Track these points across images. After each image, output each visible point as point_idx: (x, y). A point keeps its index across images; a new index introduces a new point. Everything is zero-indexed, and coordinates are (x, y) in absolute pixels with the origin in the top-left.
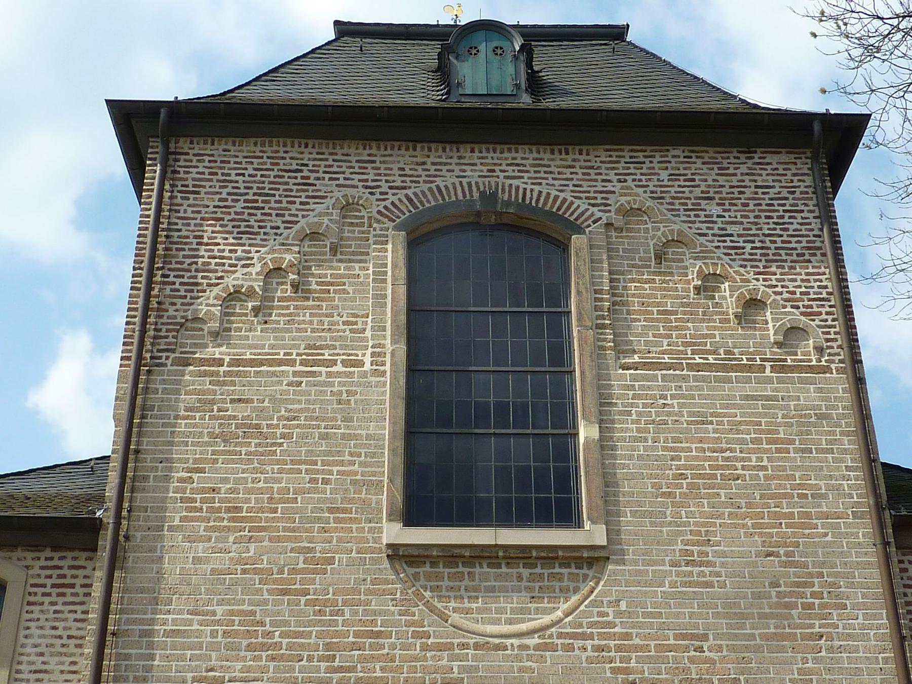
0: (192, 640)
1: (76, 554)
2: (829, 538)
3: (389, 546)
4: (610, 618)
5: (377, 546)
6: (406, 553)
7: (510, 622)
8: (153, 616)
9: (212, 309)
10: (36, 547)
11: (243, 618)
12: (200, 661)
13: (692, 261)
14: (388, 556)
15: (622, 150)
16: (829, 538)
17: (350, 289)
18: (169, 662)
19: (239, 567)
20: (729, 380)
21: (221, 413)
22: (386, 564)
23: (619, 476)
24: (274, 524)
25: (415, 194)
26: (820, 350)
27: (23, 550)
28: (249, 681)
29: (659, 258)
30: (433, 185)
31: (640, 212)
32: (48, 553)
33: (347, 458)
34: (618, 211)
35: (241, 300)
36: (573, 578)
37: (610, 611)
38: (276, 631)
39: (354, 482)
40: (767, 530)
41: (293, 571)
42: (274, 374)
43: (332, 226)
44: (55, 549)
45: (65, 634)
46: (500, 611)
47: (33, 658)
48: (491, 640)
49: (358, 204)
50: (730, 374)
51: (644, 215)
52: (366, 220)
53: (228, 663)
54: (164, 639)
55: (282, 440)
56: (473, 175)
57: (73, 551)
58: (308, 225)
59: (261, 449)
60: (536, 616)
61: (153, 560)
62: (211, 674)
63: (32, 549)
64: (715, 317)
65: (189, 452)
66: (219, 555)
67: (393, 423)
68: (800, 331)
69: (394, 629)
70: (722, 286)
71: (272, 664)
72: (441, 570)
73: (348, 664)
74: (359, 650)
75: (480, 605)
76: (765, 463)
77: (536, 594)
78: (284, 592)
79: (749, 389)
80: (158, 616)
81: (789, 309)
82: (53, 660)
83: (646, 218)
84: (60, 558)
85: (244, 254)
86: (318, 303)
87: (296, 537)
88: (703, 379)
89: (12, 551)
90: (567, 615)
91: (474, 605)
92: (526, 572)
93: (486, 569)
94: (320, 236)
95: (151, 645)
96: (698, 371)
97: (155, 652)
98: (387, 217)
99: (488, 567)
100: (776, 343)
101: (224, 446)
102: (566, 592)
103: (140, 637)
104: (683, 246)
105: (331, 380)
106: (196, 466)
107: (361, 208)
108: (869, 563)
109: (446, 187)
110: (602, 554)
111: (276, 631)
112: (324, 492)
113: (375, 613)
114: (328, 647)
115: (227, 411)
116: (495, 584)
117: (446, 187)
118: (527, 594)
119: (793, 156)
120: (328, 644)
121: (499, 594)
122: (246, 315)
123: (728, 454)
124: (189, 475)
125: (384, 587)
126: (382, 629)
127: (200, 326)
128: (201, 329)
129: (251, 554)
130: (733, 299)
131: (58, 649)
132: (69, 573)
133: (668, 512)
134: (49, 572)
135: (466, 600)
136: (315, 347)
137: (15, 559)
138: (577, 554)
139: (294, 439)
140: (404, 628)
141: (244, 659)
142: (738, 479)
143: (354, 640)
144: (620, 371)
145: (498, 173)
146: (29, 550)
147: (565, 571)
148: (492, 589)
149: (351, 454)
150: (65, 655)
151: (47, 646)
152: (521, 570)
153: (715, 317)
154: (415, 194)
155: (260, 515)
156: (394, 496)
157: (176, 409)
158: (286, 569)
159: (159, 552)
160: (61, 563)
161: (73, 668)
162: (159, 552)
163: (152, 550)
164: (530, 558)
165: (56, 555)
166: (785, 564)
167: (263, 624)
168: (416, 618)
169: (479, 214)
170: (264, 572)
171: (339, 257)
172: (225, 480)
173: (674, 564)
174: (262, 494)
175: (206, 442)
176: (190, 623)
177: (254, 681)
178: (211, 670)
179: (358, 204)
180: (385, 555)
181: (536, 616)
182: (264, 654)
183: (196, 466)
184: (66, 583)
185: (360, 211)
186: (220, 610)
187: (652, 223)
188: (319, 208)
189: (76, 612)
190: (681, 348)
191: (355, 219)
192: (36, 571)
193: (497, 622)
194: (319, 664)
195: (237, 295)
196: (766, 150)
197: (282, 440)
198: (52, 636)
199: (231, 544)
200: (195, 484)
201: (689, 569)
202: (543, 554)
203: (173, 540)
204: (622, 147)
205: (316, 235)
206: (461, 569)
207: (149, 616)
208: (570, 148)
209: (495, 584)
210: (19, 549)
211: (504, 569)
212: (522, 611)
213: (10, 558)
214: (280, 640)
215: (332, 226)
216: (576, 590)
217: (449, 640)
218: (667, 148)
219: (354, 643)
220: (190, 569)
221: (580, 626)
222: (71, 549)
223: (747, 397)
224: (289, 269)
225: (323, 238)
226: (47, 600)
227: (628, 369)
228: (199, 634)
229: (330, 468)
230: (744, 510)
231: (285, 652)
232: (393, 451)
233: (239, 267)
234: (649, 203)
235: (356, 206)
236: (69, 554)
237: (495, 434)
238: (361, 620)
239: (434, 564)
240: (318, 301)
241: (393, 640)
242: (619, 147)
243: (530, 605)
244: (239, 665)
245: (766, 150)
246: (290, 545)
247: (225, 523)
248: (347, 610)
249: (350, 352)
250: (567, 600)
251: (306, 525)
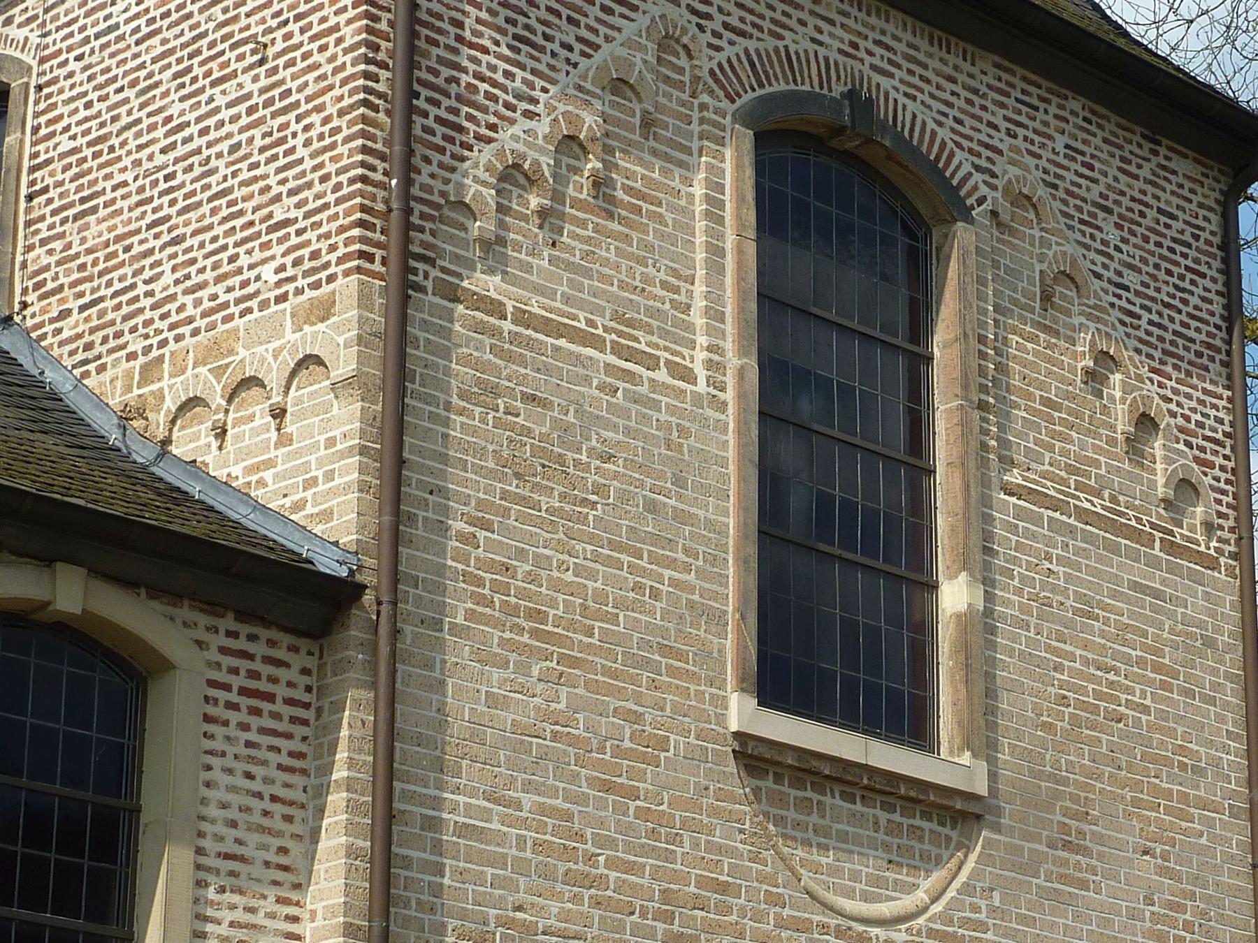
0: (492, 848)
1: (273, 634)
2: (1203, 841)
3: (738, 735)
4: (982, 916)
5: (722, 731)
6: (756, 753)
7: (866, 898)
8: (437, 792)
9: (485, 191)
10: (213, 607)
11: (558, 823)
12: (503, 889)
13: (1083, 320)
14: (734, 751)
15: (1133, 132)
16: (1203, 841)
17: (669, 217)
18: (464, 883)
19: (549, 728)
20: (1114, 549)
21: (509, 417)
22: (732, 767)
23: (998, 681)
24: (591, 658)
25: (757, 51)
26: (1209, 527)
27: (192, 608)
28: (569, 938)
29: (1047, 297)
30: (781, 44)
31: (1026, 203)
32: (229, 622)
33: (681, 556)
34: (1007, 191)
35: (518, 185)
36: (936, 839)
37: (983, 904)
38: (599, 855)
39: (691, 605)
40: (1144, 812)
41: (618, 752)
42: (578, 360)
43: (649, 76)
44: (242, 617)
45: (267, 791)
46: (855, 876)
47: (221, 829)
48: (853, 924)
49: (677, 41)
50: (1119, 539)
51: (1031, 210)
52: (687, 79)
53: (540, 899)
54: (454, 839)
55: (594, 498)
56: (834, 42)
57: (269, 628)
58: (616, 59)
59: (567, 508)
60: (894, 894)
61: (431, 686)
62: (519, 915)
63: (206, 607)
64: (1101, 431)
65: (469, 484)
66: (520, 696)
67: (742, 508)
68: (1190, 490)
69: (745, 883)
70: (1111, 376)
71: (597, 913)
72: (786, 789)
73: (690, 931)
74: (702, 909)
75: (830, 860)
76: (1148, 702)
77: (789, 831)
78: (608, 788)
79: (1137, 572)
80: (446, 795)
81: (1181, 446)
82: (253, 838)
83: (1032, 216)
84: (252, 638)
85: (524, 88)
86: (626, 231)
87: (620, 689)
88: (1089, 538)
89: (175, 605)
90: (934, 900)
91: (824, 860)
92: (883, 816)
93: (838, 802)
94: (626, 88)
95: (438, 847)
96: (1087, 523)
97: (445, 861)
98: (723, 87)
99: (921, 818)
100: (1163, 500)
101: (517, 486)
102: (930, 862)
103: (422, 829)
104: (1072, 286)
105: (655, 396)
106: (480, 514)
107: (680, 50)
108: (1239, 889)
109: (797, 53)
110: (973, 808)
111: (599, 855)
112: (652, 613)
113: (720, 849)
114: (666, 896)
115: (517, 415)
116: (848, 828)
117: (797, 53)
118: (884, 855)
119: (1200, 169)
120: (665, 891)
121: (853, 848)
122: (525, 218)
123: (1111, 676)
124: (472, 529)
125: (730, 807)
126: (730, 879)
127: (462, 219)
128: (464, 229)
129: (562, 706)
130: (1126, 407)
131: (257, 818)
132: (266, 670)
133: (1048, 757)
134: (235, 662)
135: (815, 850)
136: (630, 323)
137: (179, 621)
138: (945, 802)
139: (611, 500)
140: (755, 884)
141: (559, 897)
142: (1119, 721)
143: (696, 891)
144: (1002, 496)
145: (862, 54)
146: (202, 610)
147: (926, 825)
148: (843, 837)
149: (686, 551)
150: (269, 833)
151: (241, 810)
152: (878, 812)
153: (1101, 431)
154: (757, 51)
155: (570, 634)
156: (746, 647)
157: (447, 391)
158: (608, 744)
159: (438, 671)
160: (251, 648)
161: (283, 860)
162: (438, 671)
163: (429, 665)
164: (855, 784)
165: (244, 629)
166: (1162, 871)
167: (581, 838)
168: (768, 869)
169: (839, 131)
170: (581, 745)
171: (652, 143)
172: (521, 554)
173: (1051, 846)
174: (572, 594)
175: (491, 471)
176: (486, 815)
177: (573, 938)
178: (519, 908)
179: (677, 41)
180: (730, 749)
181: (894, 894)
182: (586, 894)
183: (480, 514)
184: (262, 689)
185: (677, 55)
186: (528, 800)
187: (1042, 229)
188: (629, 28)
189: (279, 751)
190: (1063, 474)
191: (673, 71)
192: (213, 655)
193: (850, 894)
194: (654, 923)
195: (513, 171)
196: (1176, 146)
197: (594, 498)
198: (248, 791)
199: (535, 680)
200: (481, 550)
201: (1065, 854)
202: (913, 794)
203: (459, 653)
204: (1015, 68)
205: (622, 85)
206: (809, 794)
207: (431, 792)
208: (953, 40)
209: (848, 828)
210: (186, 602)
211: (859, 807)
212: (878, 882)
213: (172, 619)
214: (606, 872)
215: (649, 76)
216: (939, 862)
217: (806, 915)
218: (1067, 93)
219: (697, 897)
220: (483, 713)
221: (951, 922)
222: (266, 622)
223: (1135, 586)
224: (590, 147)
225: (629, 94)
226: (234, 717)
227: (1011, 494)
228: (502, 839)
229: (660, 570)
230: (1124, 773)
231: (612, 894)
232: (742, 561)
233: (518, 115)
234: (1042, 192)
235: (673, 43)
236: (264, 633)
237: (840, 558)
238: (703, 858)
239: (778, 778)
240: (626, 226)
241: (742, 901)
242: (1185, 150)
243: (887, 874)
244: (555, 907)
245: (1176, 146)
246: (614, 703)
247: (525, 638)
248: (686, 836)
249: (625, 329)
250: (928, 872)
251: (632, 670)
